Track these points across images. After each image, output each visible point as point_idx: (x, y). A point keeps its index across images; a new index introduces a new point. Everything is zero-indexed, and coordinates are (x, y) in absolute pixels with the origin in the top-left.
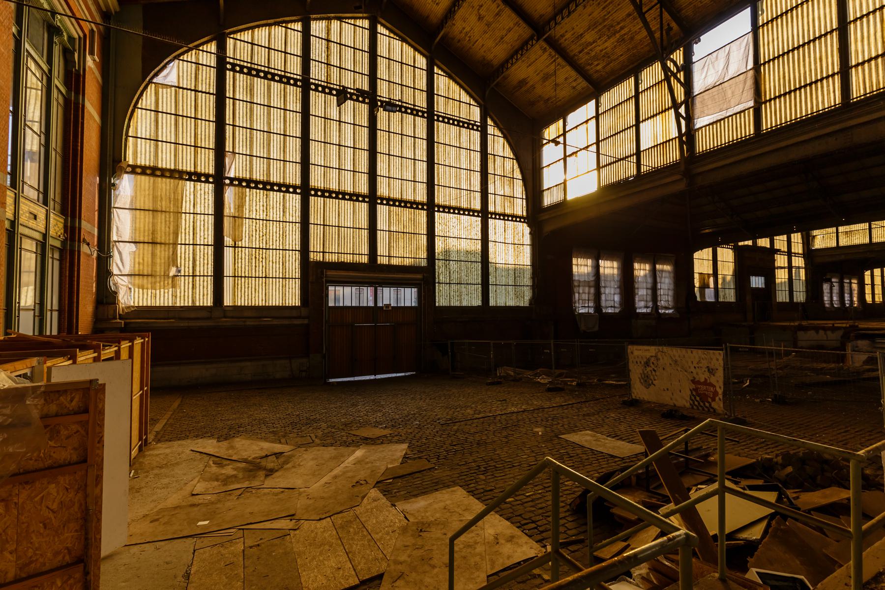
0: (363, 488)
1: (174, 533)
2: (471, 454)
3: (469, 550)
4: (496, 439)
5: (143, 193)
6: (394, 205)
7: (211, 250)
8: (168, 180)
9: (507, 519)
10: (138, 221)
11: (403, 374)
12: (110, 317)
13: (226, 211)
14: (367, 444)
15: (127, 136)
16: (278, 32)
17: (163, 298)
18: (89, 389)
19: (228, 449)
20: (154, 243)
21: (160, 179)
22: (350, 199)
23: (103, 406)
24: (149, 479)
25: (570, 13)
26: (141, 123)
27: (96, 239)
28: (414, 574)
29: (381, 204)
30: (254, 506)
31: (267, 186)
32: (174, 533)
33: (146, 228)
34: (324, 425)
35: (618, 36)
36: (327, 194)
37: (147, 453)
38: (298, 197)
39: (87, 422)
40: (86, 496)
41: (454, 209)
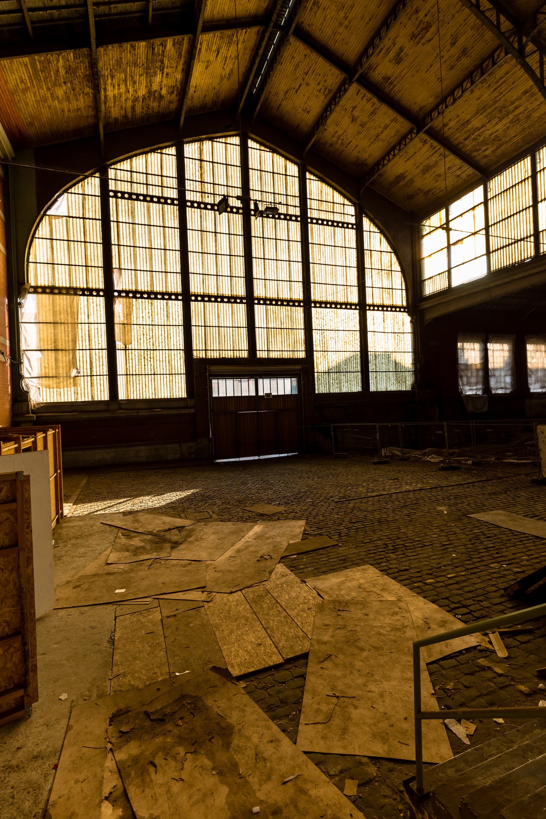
0: (269, 563)
1: (95, 599)
2: (374, 531)
3: (398, 634)
4: (397, 517)
5: (44, 309)
6: (271, 304)
7: (105, 353)
8: (65, 296)
9: (434, 602)
10: (42, 332)
11: (286, 455)
12: (24, 412)
13: (117, 320)
14: (264, 520)
15: (28, 262)
16: (154, 157)
17: (67, 395)
18: (15, 480)
20: (56, 350)
21: (57, 296)
22: (229, 302)
23: (29, 495)
24: (67, 548)
25: (455, 100)
26: (39, 250)
27: (8, 349)
28: (341, 656)
29: (259, 303)
30: (166, 577)
31: (152, 295)
32: (95, 599)
33: (49, 338)
34: (219, 502)
35: (511, 116)
36: (206, 299)
37: (64, 525)
38: (180, 303)
39: (16, 510)
40: (19, 577)
41: (331, 304)
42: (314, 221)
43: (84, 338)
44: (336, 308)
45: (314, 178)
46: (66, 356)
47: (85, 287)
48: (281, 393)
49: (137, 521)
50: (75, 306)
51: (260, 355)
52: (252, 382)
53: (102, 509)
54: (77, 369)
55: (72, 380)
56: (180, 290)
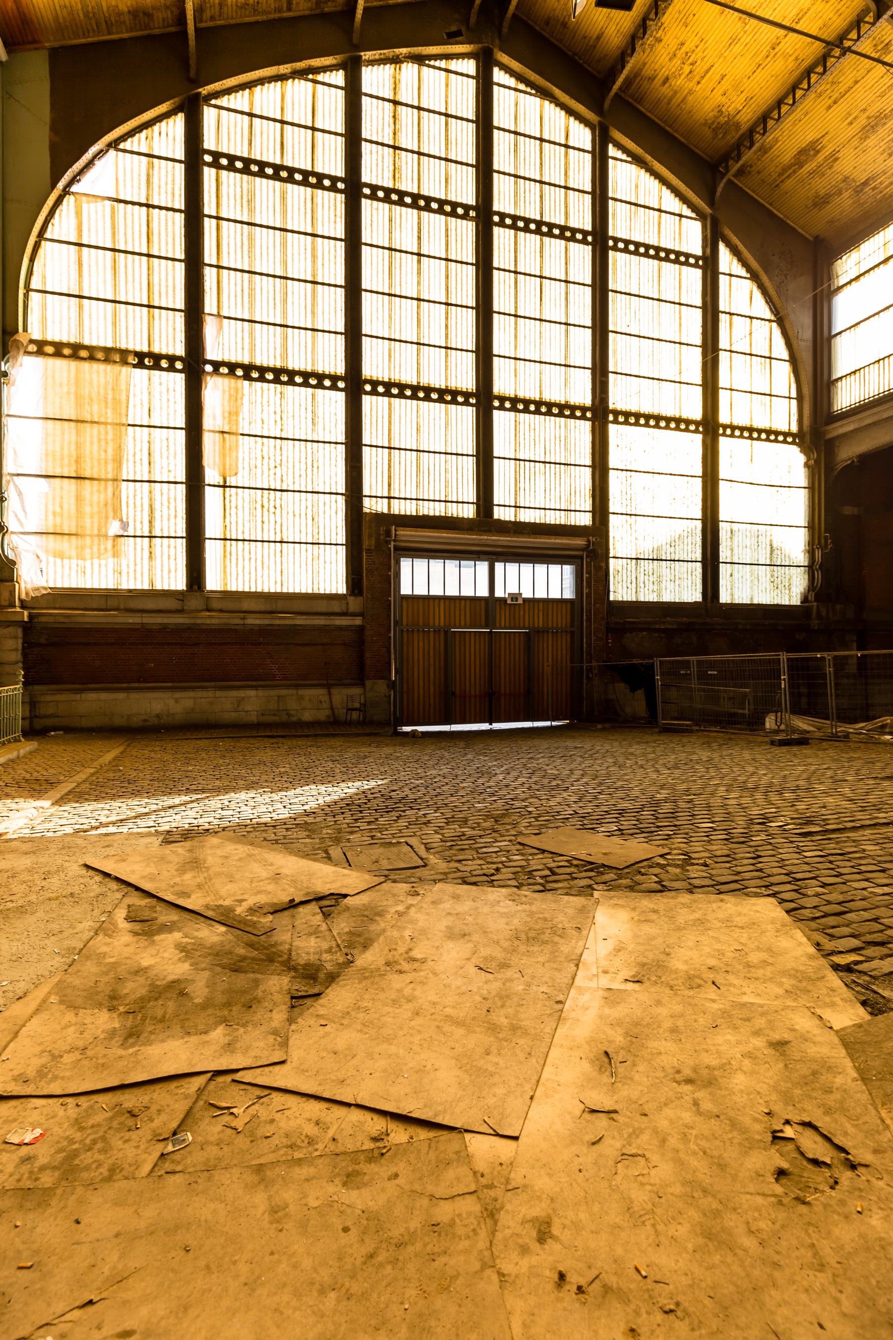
6: (526, 410)
7: (181, 490)
16: (299, 89)
19: (182, 870)
29: (502, 408)
31: (283, 376)
33: (66, 452)
38: (341, 396)
41: (648, 417)
42: (621, 245)
43: (138, 457)
44: (657, 426)
45: (624, 157)
46: (99, 491)
47: (145, 349)
48: (541, 594)
49: (195, 864)
50: (123, 387)
51: (499, 514)
52: (483, 567)
53: (114, 823)
54: (121, 520)
55: (110, 543)
56: (341, 370)
